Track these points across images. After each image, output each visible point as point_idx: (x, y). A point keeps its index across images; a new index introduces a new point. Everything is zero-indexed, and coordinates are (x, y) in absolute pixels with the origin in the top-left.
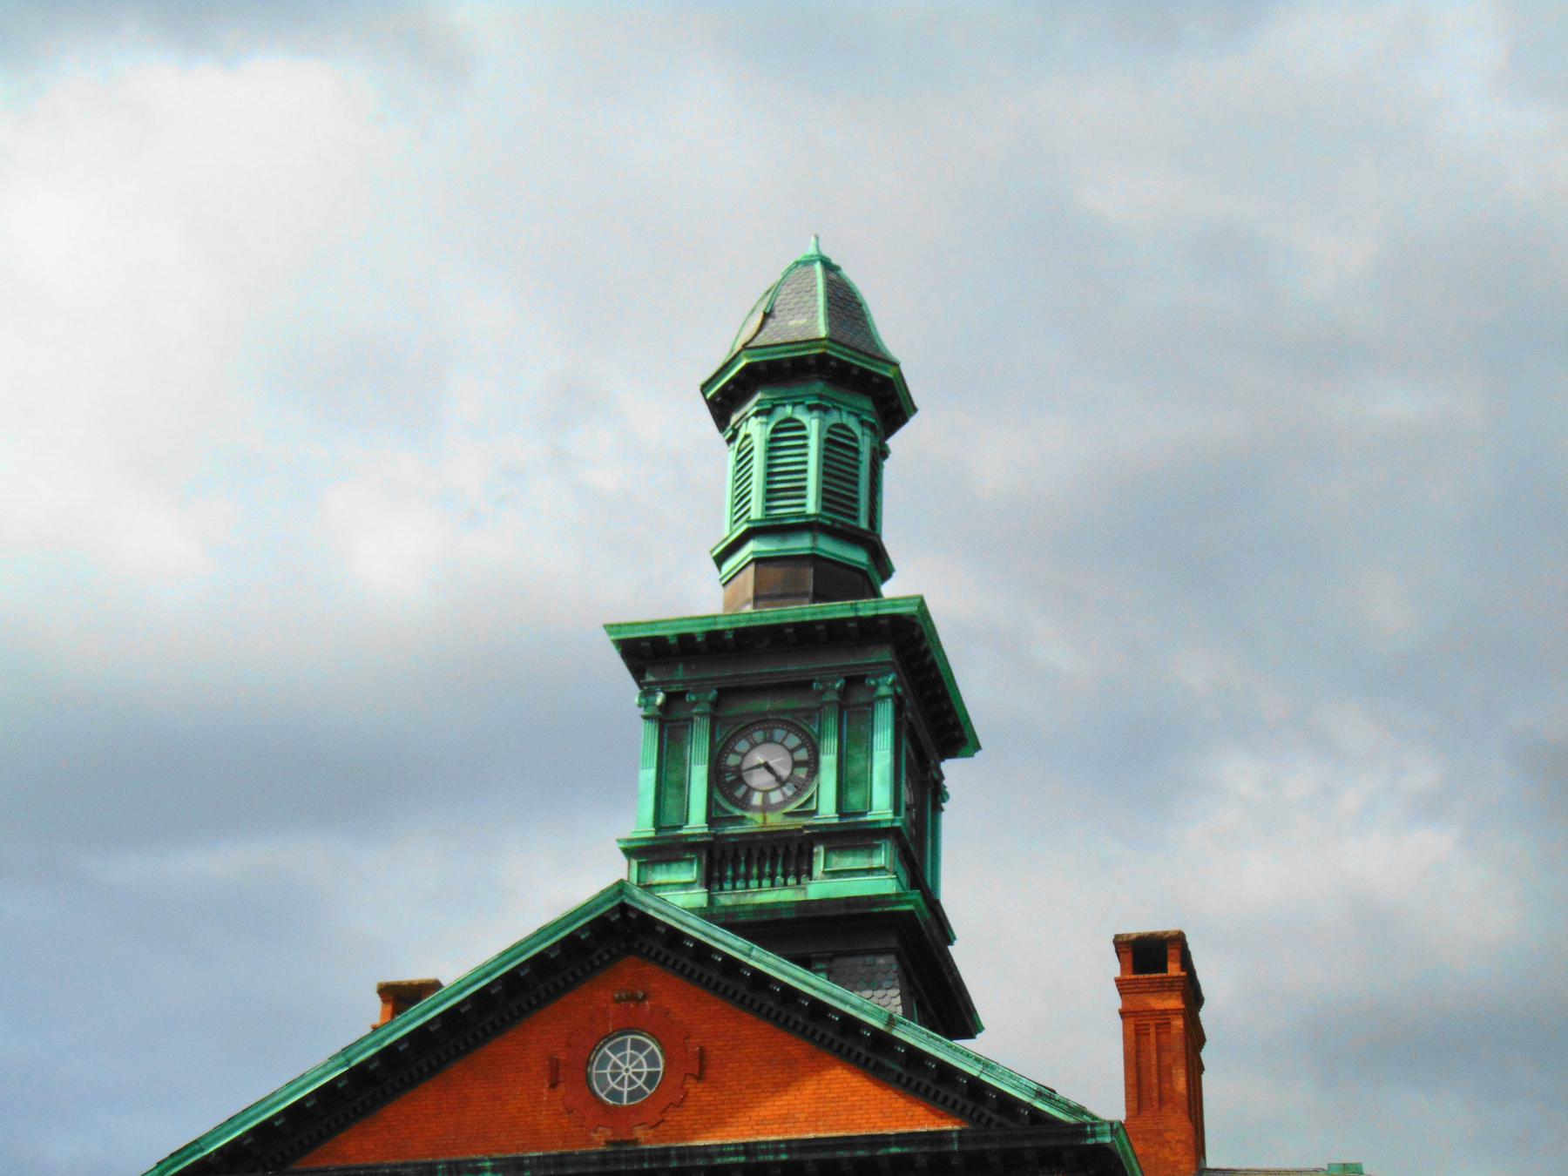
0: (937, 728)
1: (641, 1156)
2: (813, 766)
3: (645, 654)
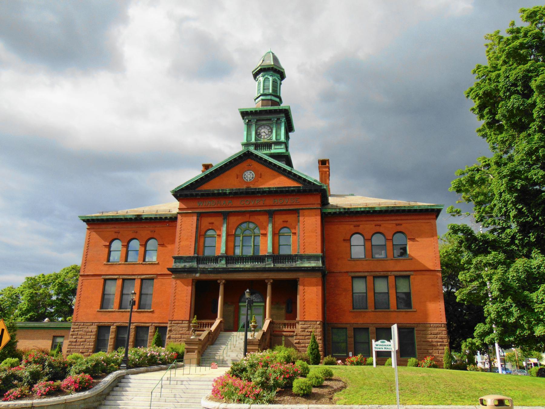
0: (289, 128)
1: (252, 189)
2: (272, 132)
3: (244, 114)
